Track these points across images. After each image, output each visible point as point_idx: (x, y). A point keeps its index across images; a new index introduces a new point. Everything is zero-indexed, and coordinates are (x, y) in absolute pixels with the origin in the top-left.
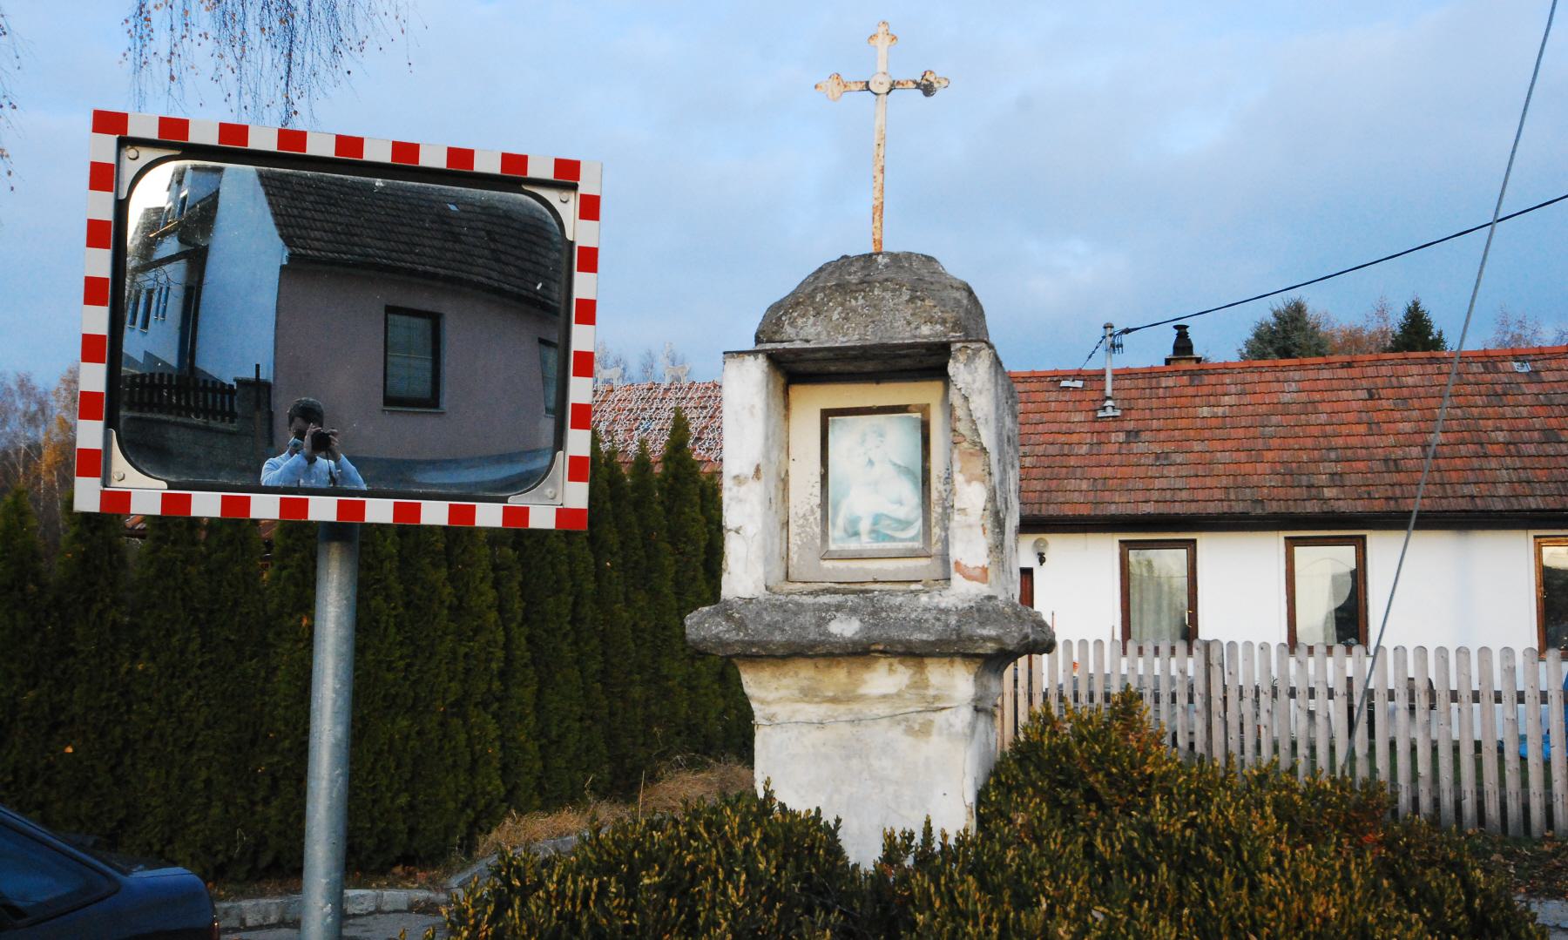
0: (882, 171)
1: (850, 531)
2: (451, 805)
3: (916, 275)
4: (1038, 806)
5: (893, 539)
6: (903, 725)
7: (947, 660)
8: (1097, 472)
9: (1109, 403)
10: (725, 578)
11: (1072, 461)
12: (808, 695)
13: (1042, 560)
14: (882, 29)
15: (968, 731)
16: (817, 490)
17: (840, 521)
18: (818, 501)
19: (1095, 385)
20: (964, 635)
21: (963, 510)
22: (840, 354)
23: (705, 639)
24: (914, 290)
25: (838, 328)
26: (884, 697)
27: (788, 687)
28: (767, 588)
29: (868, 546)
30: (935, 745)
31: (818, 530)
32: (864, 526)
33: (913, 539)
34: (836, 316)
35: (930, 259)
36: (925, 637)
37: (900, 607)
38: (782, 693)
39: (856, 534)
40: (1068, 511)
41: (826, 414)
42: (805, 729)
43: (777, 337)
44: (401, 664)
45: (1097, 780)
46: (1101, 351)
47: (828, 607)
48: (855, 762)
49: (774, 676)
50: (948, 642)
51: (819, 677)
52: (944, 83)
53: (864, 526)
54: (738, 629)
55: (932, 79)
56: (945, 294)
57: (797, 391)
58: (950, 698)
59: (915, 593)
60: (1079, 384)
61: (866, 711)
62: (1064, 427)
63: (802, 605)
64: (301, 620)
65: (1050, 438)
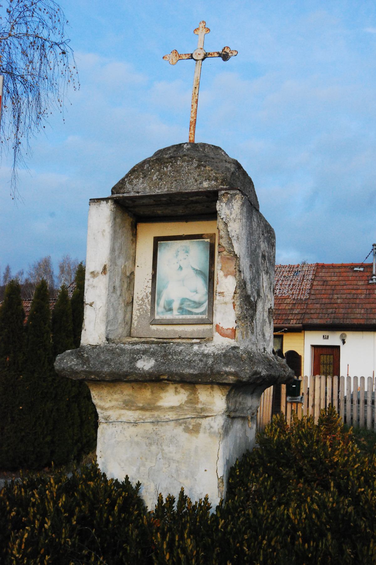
0: (197, 102)
1: (167, 308)
2: (70, 441)
3: (203, 155)
4: (266, 479)
5: (190, 313)
6: (183, 427)
7: (209, 386)
8: (368, 306)
9: (374, 277)
10: (83, 332)
11: (358, 301)
12: (128, 405)
13: (344, 342)
14: (203, 25)
15: (221, 431)
16: (150, 284)
17: (162, 302)
18: (150, 290)
19: (368, 270)
20: (215, 371)
21: (221, 293)
22: (157, 199)
23: (64, 369)
24: (200, 160)
25: (156, 185)
26: (172, 408)
27: (117, 400)
28: (108, 339)
29: (177, 317)
30: (202, 439)
31: (149, 307)
32: (175, 305)
33: (202, 313)
34: (155, 177)
35: (217, 148)
36: (191, 371)
37: (180, 353)
38: (114, 403)
39: (171, 310)
40: (355, 322)
41: (157, 240)
42: (126, 426)
43: (122, 191)
44: (50, 379)
45: (304, 464)
46: (371, 256)
47: (138, 352)
48: (154, 448)
49: (108, 393)
50: (206, 375)
51: (135, 394)
52: (235, 53)
53: (175, 305)
54: (84, 364)
55: (228, 51)
56: (219, 165)
57: (142, 228)
58: (212, 411)
59: (192, 344)
60: (362, 269)
61: (162, 416)
62: (355, 287)
63: (124, 350)
64: (6, 359)
65: (349, 291)
